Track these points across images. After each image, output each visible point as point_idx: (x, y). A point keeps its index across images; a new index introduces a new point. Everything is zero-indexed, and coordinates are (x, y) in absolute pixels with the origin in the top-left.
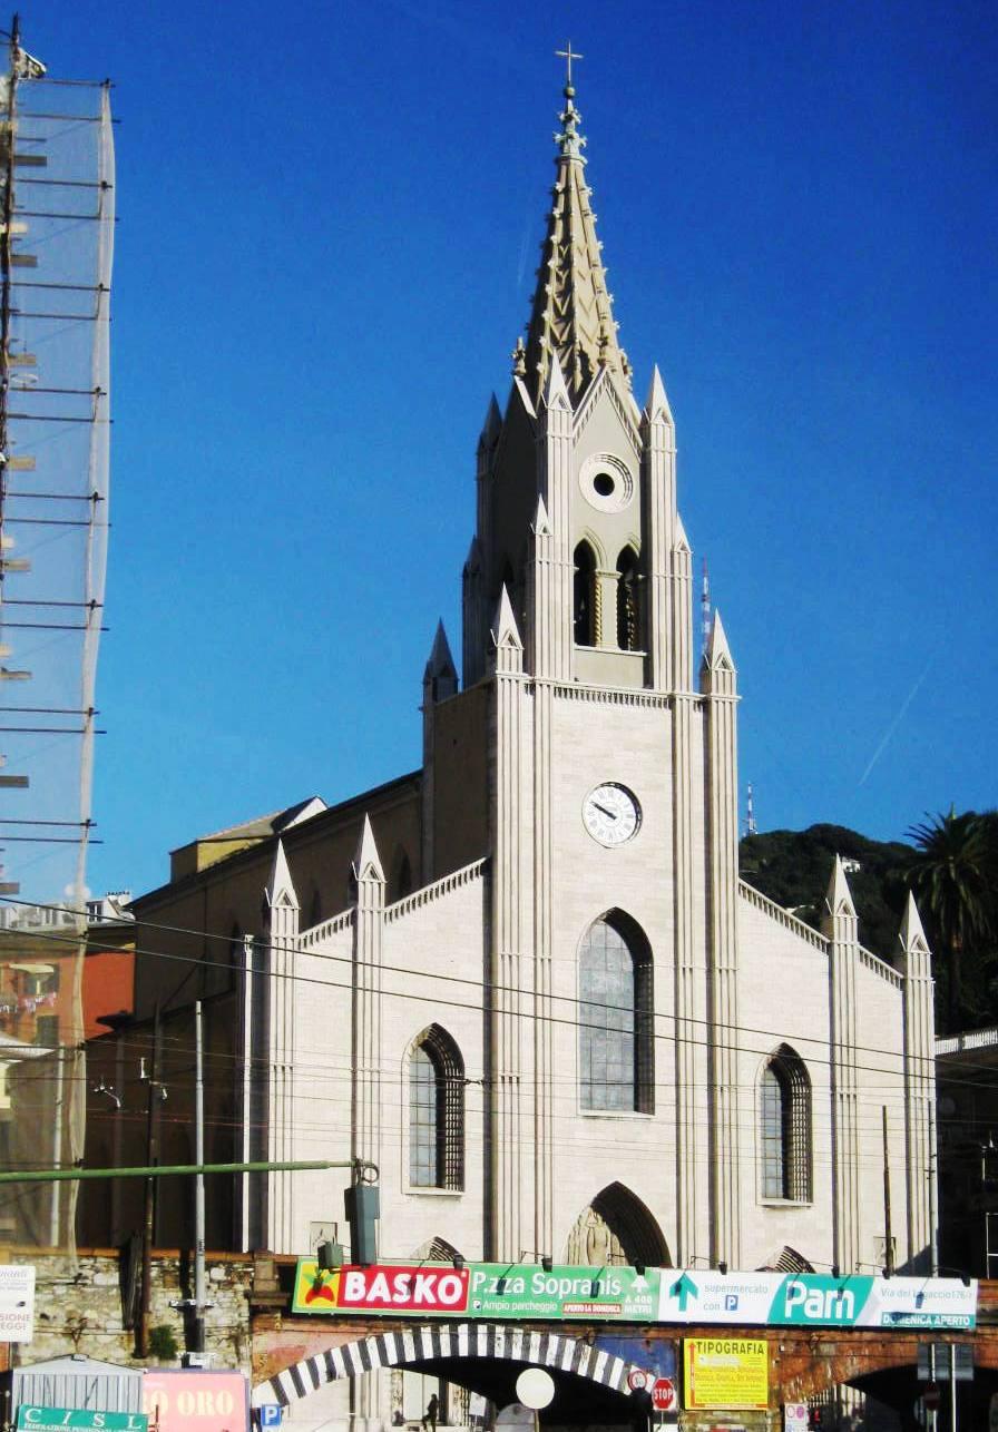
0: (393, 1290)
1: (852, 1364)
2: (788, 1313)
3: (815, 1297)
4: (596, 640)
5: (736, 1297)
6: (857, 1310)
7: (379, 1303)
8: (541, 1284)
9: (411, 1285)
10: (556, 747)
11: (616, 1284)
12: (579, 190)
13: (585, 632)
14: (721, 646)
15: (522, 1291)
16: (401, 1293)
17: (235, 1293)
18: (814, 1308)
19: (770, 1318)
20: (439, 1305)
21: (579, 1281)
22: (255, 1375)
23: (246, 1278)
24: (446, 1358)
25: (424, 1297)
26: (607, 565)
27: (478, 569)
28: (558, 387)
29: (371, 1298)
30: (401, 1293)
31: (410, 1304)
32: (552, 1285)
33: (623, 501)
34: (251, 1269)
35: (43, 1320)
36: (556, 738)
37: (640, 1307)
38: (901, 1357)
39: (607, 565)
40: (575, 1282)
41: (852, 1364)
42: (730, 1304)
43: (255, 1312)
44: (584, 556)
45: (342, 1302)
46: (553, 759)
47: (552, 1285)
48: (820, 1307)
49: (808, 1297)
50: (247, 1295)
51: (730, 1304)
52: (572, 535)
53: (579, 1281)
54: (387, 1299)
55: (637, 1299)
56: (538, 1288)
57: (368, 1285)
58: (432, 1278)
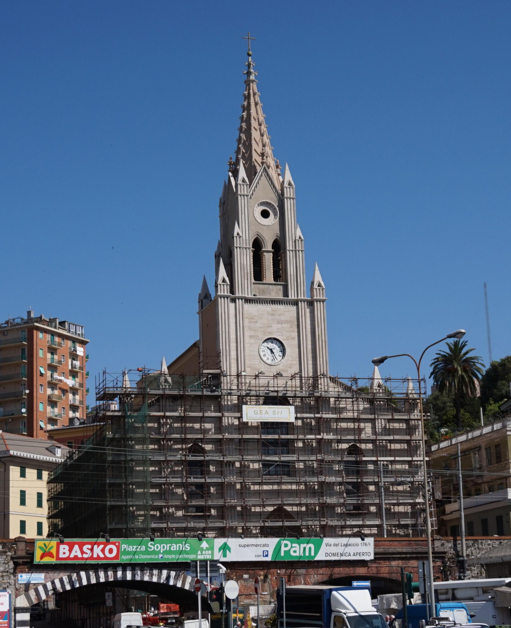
0: (83, 552)
1: (314, 578)
2: (282, 554)
3: (296, 547)
4: (263, 279)
5: (267, 551)
6: (316, 553)
7: (76, 557)
8: (152, 547)
9: (92, 550)
10: (246, 324)
11: (188, 546)
12: (254, 94)
13: (258, 275)
14: (318, 278)
15: (144, 550)
16: (86, 553)
17: (7, 556)
18: (295, 552)
19: (272, 559)
20: (106, 558)
21: (170, 545)
22: (17, 592)
23: (13, 549)
24: (186, 590)
25: (98, 555)
26: (268, 246)
27: (220, 254)
28: (242, 173)
29: (72, 556)
30: (86, 553)
31: (92, 558)
32: (157, 547)
33: (272, 221)
34: (14, 546)
35: (473, 618)
36: (246, 321)
37: (205, 556)
38: (339, 574)
39: (268, 246)
40: (168, 545)
41: (314, 578)
42: (265, 554)
43: (16, 564)
44: (257, 244)
45: (58, 558)
46: (245, 329)
47: (157, 547)
48: (298, 552)
49: (292, 547)
50: (12, 558)
51: (265, 554)
52: (250, 235)
53: (170, 545)
54: (80, 556)
55: (204, 552)
56: (151, 548)
57: (70, 551)
58: (102, 546)
